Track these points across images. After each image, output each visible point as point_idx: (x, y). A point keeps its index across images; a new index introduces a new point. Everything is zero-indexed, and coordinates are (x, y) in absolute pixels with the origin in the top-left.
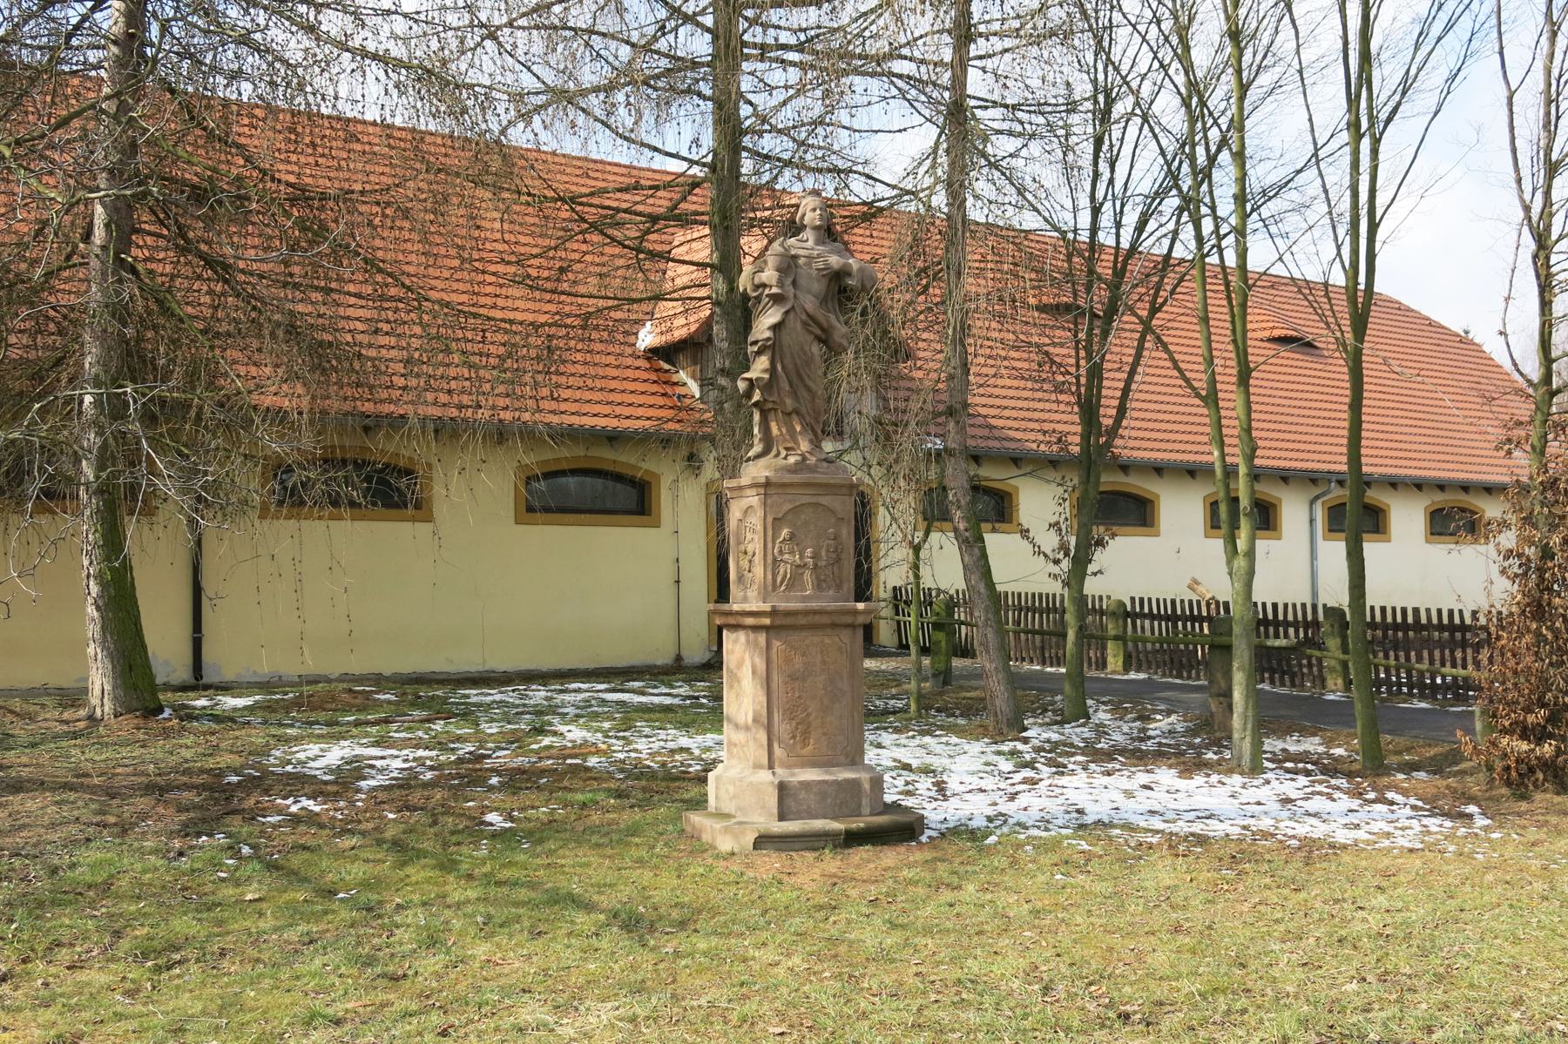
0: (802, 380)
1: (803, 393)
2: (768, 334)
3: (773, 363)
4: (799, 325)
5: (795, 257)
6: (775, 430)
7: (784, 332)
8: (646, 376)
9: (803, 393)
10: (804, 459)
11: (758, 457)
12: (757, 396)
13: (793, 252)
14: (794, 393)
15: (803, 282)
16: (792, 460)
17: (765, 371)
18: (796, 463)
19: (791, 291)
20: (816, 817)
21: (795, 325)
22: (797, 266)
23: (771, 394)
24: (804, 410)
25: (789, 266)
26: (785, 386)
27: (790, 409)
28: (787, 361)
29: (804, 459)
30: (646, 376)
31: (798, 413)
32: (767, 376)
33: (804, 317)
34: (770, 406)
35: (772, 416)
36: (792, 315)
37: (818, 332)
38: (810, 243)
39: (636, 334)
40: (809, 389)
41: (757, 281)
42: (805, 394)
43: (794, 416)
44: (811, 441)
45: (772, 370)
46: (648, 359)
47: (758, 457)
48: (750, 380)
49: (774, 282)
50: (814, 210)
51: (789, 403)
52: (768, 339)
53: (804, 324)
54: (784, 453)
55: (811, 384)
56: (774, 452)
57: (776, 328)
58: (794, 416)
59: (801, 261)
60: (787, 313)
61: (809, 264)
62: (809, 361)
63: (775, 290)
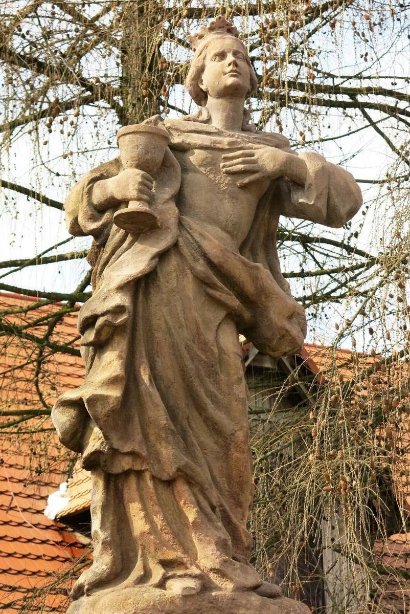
0: (200, 408)
1: (201, 435)
2: (119, 299)
3: (130, 366)
4: (190, 286)
5: (181, 150)
6: (139, 525)
7: (155, 298)
8: (55, 551)
9: (201, 435)
10: (206, 587)
11: (100, 584)
12: (95, 441)
13: (176, 139)
14: (180, 433)
15: (198, 198)
16: (176, 587)
17: (113, 381)
18: (186, 596)
19: (169, 213)
20: (315, 220)
21: (179, 284)
22: (186, 168)
23: (126, 437)
24: (204, 475)
25: (165, 164)
26: (158, 414)
27: (170, 470)
28: (165, 363)
29: (206, 587)
30: (55, 551)
31: (190, 481)
32: (115, 393)
33: (201, 267)
34: (125, 464)
35: (131, 488)
36: (173, 262)
37: (234, 302)
38: (217, 123)
39: (44, 498)
40: (215, 428)
41: (98, 196)
42: (209, 441)
43: (182, 488)
44: (222, 545)
45: (129, 380)
46: (60, 530)
47: (100, 584)
48: (77, 404)
49: (132, 192)
50: (222, 55)
51: (169, 455)
52: (119, 310)
53: (203, 282)
54: (158, 573)
55: (219, 415)
56: (137, 572)
57: (139, 286)
58: (182, 488)
59: (195, 157)
60: (162, 256)
61: (211, 164)
62: (214, 366)
63: (133, 206)
